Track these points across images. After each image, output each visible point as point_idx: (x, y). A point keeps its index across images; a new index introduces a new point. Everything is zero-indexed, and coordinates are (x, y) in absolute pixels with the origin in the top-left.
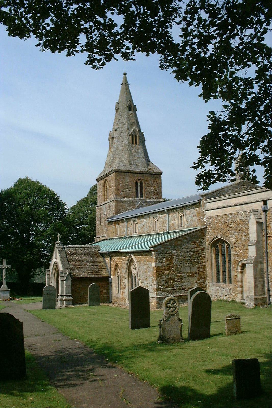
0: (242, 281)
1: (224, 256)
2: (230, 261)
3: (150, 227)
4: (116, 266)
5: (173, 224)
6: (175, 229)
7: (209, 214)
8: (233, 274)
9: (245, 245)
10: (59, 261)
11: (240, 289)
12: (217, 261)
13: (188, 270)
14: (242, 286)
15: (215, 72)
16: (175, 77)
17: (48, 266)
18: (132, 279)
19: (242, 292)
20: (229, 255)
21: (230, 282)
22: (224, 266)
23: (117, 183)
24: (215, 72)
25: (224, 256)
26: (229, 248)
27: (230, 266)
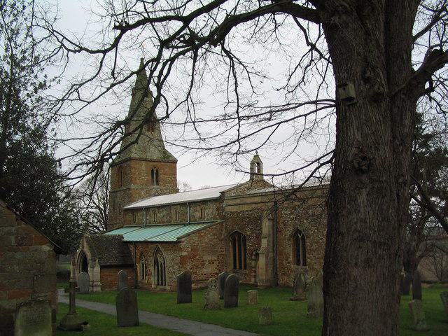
0: (255, 267)
1: (240, 245)
2: (245, 249)
3: (170, 217)
4: (142, 254)
5: (194, 216)
6: (196, 220)
7: (228, 209)
8: (248, 261)
9: (259, 237)
10: (86, 250)
11: (253, 274)
12: (234, 250)
13: (209, 258)
14: (255, 272)
15: (314, 8)
16: (137, 324)
17: (74, 252)
18: (158, 266)
19: (255, 277)
20: (245, 245)
21: (245, 268)
22: (240, 255)
23: (155, 134)
24: (314, 8)
25: (240, 245)
26: (245, 240)
27: (245, 255)
